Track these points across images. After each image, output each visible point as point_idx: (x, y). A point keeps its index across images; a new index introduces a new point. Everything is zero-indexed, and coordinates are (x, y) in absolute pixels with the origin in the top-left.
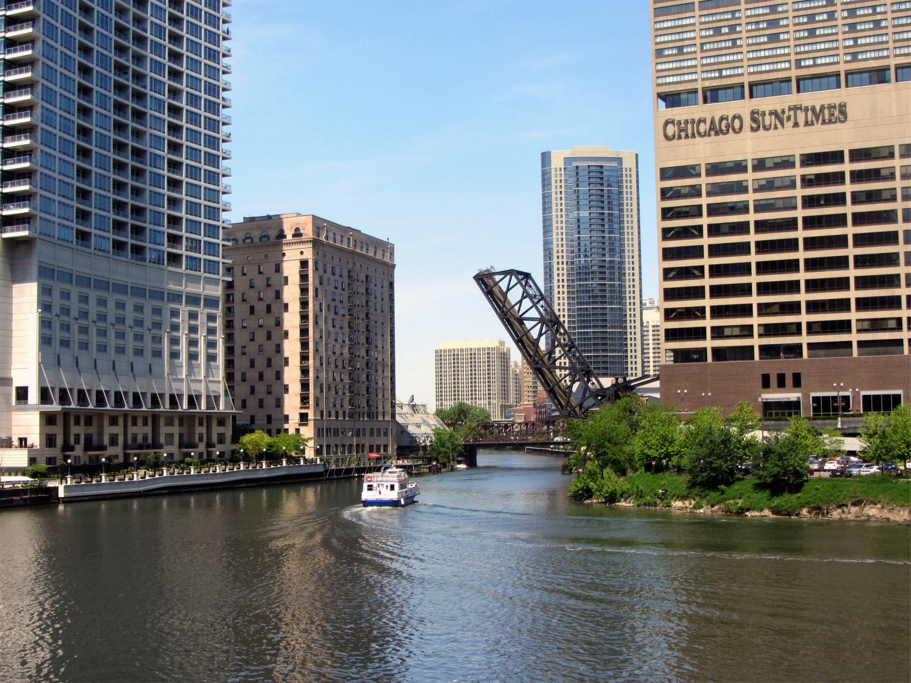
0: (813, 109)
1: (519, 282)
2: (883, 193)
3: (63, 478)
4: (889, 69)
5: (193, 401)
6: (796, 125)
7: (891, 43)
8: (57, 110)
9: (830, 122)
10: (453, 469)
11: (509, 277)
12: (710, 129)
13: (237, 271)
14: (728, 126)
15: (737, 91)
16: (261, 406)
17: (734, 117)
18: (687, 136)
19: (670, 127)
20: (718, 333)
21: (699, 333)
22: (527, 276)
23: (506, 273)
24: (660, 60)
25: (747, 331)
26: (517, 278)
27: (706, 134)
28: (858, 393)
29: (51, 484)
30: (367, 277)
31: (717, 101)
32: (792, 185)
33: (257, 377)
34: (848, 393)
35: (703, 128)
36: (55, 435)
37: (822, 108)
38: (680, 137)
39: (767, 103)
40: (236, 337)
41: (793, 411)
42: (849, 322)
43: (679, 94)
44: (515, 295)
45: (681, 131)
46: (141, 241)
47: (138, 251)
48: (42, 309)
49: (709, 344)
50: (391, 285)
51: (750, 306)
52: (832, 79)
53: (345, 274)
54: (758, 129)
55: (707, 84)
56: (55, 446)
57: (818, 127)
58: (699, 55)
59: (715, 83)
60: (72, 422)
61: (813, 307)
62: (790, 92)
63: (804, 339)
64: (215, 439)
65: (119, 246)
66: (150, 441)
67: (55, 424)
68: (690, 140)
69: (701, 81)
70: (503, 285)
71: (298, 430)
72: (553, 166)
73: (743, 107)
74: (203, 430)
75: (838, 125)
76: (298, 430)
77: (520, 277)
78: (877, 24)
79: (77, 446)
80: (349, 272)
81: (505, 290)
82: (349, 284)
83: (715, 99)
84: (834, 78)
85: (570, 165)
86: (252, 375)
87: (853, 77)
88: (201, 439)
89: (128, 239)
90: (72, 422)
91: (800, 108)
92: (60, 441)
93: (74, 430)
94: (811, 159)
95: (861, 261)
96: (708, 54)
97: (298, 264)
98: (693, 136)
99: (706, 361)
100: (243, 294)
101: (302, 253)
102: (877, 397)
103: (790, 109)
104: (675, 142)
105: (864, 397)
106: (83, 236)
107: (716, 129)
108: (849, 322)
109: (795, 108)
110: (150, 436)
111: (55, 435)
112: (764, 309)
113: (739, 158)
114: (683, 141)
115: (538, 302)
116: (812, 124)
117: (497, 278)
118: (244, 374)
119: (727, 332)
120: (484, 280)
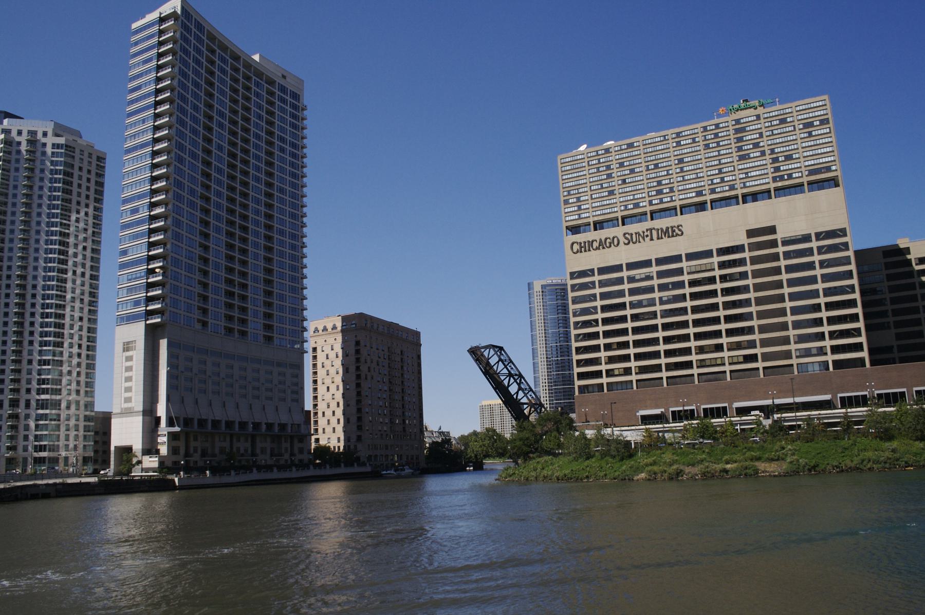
0: (662, 229)
1: (496, 353)
2: (812, 349)
3: (178, 474)
4: (707, 203)
5: (283, 427)
6: (652, 239)
7: (706, 186)
8: (183, 246)
9: (673, 236)
10: (466, 470)
11: (488, 350)
12: (600, 245)
13: (319, 350)
14: (610, 243)
15: (612, 222)
16: (334, 432)
17: (614, 238)
18: (585, 251)
19: (575, 245)
20: (610, 373)
21: (598, 374)
22: (501, 349)
23: (486, 347)
24: (566, 206)
25: (627, 371)
26: (495, 350)
27: (598, 248)
28: (700, 406)
29: (170, 477)
30: (402, 352)
31: (603, 229)
32: (651, 278)
33: (331, 413)
34: (693, 407)
35: (595, 245)
36: (179, 447)
37: (668, 228)
38: (581, 252)
39: (633, 228)
40: (355, 393)
41: (660, 421)
42: (691, 362)
43: (580, 227)
44: (513, 389)
45: (581, 247)
46: (245, 328)
47: (243, 334)
48: (170, 368)
49: (604, 380)
50: (419, 357)
51: (629, 355)
52: (669, 211)
53: (386, 350)
54: (629, 243)
55: (596, 219)
56: (179, 454)
57: (665, 239)
58: (590, 201)
59: (601, 218)
60: (192, 439)
61: (669, 353)
62: (646, 220)
63: (664, 374)
64: (296, 451)
65: (230, 331)
66: (249, 451)
67: (179, 440)
68: (588, 253)
69: (590, 217)
70: (486, 354)
71: (355, 446)
72: (535, 290)
73: (617, 232)
74: (288, 445)
75: (678, 238)
76: (355, 446)
77: (496, 350)
78: (681, 161)
79: (195, 454)
80: (389, 348)
81: (500, 362)
82: (389, 356)
83: (602, 228)
84: (674, 211)
85: (545, 289)
86: (329, 413)
87: (684, 209)
88: (286, 449)
89: (236, 326)
90: (192, 439)
91: (654, 229)
92: (182, 451)
93: (193, 444)
94: (660, 261)
95: (697, 323)
96: (596, 200)
97: (354, 343)
98: (589, 250)
99: (603, 391)
100: (323, 363)
101: (356, 336)
102: (712, 409)
103: (647, 230)
104: (579, 254)
105: (704, 409)
106: (205, 324)
107: (602, 245)
108: (691, 362)
109: (651, 230)
110: (235, 440)
111: (179, 447)
112: (638, 357)
113: (618, 263)
114: (584, 254)
115: (508, 364)
116: (662, 238)
117: (483, 350)
118: (324, 429)
119: (616, 372)
120: (475, 352)
